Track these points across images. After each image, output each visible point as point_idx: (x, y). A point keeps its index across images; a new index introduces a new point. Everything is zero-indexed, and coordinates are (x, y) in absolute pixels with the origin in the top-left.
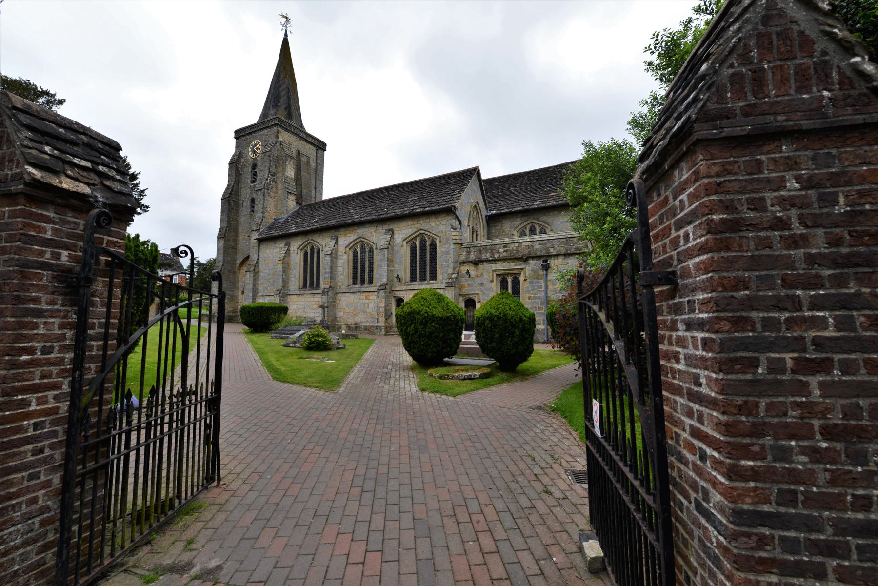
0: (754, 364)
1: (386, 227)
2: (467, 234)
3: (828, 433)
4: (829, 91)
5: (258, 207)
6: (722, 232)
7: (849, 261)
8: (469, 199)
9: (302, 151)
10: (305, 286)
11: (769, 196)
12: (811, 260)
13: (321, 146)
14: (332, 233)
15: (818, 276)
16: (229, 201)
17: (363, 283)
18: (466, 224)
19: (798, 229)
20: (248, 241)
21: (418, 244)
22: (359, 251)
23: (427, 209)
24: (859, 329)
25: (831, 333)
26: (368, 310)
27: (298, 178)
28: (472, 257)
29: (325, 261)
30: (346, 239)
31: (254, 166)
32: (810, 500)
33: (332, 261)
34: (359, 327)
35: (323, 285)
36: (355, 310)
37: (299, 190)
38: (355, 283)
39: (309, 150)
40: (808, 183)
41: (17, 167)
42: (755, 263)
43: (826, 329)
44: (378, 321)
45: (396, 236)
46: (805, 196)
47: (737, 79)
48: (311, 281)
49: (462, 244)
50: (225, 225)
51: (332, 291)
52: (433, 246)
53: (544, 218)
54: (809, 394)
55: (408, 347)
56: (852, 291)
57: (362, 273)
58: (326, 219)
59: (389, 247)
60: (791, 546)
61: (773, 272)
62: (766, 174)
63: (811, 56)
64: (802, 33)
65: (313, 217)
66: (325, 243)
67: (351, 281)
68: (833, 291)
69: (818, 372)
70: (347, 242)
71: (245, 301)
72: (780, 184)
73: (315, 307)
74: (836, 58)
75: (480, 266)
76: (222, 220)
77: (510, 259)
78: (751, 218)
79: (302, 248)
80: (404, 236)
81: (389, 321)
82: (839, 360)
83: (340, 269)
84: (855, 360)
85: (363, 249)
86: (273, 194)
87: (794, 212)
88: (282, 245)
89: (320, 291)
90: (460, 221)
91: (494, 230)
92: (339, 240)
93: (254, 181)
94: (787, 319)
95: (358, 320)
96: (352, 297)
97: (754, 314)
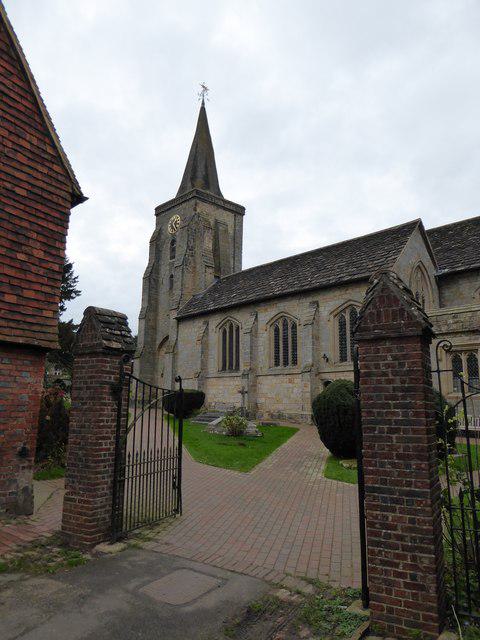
1: (310, 299)
3: (399, 457)
5: (177, 285)
7: (408, 390)
9: (220, 219)
10: (224, 368)
12: (394, 388)
13: (238, 211)
14: (250, 310)
17: (286, 363)
19: (391, 377)
20: (167, 321)
23: (356, 277)
25: (400, 418)
27: (216, 250)
29: (244, 339)
30: (267, 314)
31: (173, 242)
32: (392, 483)
33: (251, 339)
35: (242, 367)
37: (217, 261)
38: (277, 364)
39: (227, 218)
40: (395, 358)
42: (375, 390)
45: (321, 309)
47: (371, 314)
48: (230, 363)
51: (252, 373)
55: (324, 438)
57: (285, 352)
58: (246, 292)
60: (385, 500)
65: (232, 292)
66: (244, 319)
67: (273, 361)
70: (268, 318)
71: (166, 384)
72: (385, 358)
77: (463, 332)
79: (221, 326)
85: (285, 325)
88: (201, 324)
89: (240, 374)
91: (447, 293)
93: (173, 257)
95: (281, 407)
96: (274, 380)
97: (374, 410)
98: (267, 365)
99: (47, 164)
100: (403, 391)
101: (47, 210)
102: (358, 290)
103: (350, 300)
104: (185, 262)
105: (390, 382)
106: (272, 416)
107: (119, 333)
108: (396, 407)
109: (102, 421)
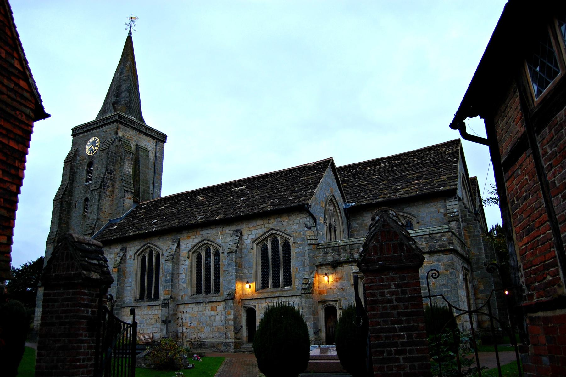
0: (382, 353)
1: (234, 228)
2: (323, 232)
8: (327, 187)
10: (142, 298)
11: (386, 291)
12: (399, 314)
13: (161, 138)
15: (401, 320)
16: (62, 202)
17: (208, 291)
18: (322, 221)
19: (395, 303)
21: (269, 246)
22: (203, 255)
25: (405, 340)
26: (215, 324)
28: (330, 258)
29: (165, 266)
30: (189, 242)
31: (90, 164)
34: (204, 344)
35: (162, 296)
36: (199, 323)
39: (148, 144)
40: (397, 286)
41: (77, 270)
43: (404, 338)
44: (226, 337)
45: (245, 237)
46: (397, 291)
49: (318, 245)
50: (56, 229)
51: (173, 303)
52: (287, 246)
53: (409, 209)
54: (399, 362)
57: (208, 281)
59: (237, 250)
62: (385, 283)
63: (397, 240)
64: (394, 231)
66: (165, 246)
67: (194, 289)
70: (190, 245)
72: (389, 287)
73: (153, 321)
75: (340, 269)
76: (52, 223)
80: (254, 237)
81: (239, 335)
83: (183, 276)
86: (108, 193)
87: (393, 297)
90: (314, 219)
91: (354, 225)
92: (181, 243)
95: (202, 336)
97: (382, 334)
98: (189, 294)
99: (13, 78)
101: (8, 126)
102: (279, 219)
103: (272, 229)
104: (103, 185)
105: (394, 308)
106: (192, 345)
107: (96, 262)
108: (401, 330)
109: (79, 360)
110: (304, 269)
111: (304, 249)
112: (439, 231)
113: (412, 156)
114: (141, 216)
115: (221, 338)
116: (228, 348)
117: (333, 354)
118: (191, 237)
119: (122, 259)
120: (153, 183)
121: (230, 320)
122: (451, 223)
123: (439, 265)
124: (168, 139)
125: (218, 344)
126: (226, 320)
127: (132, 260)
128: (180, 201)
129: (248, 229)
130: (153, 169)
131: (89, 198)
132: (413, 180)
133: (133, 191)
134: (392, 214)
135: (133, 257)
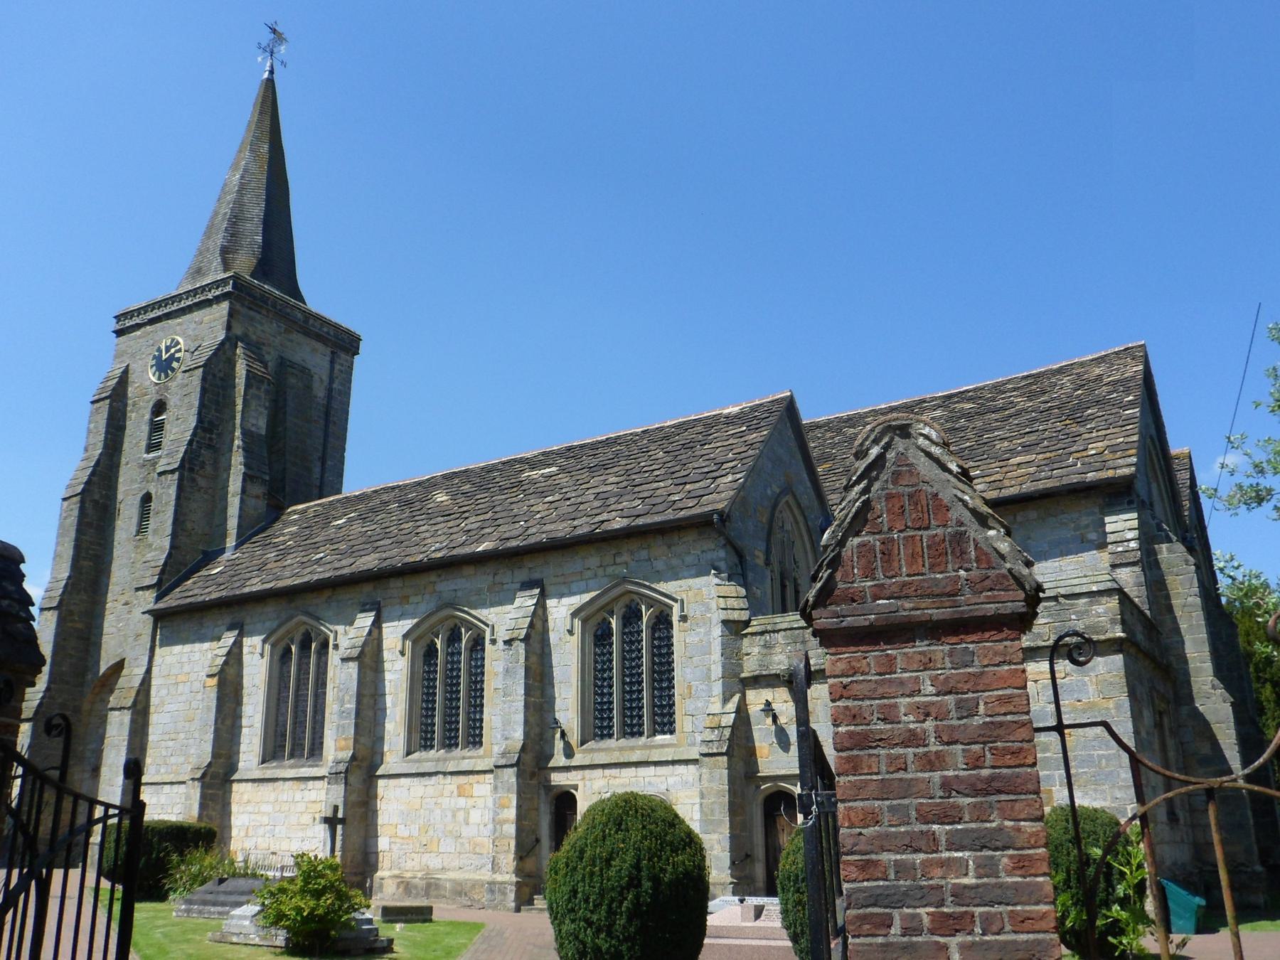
4: (967, 570)
6: (848, 749)
12: (946, 785)
13: (344, 344)
18: (760, 561)
19: (934, 747)
23: (640, 521)
24: (1002, 874)
26: (466, 831)
31: (160, 407)
34: (437, 886)
36: (425, 829)
39: (315, 358)
44: (495, 867)
46: (941, 704)
51: (363, 773)
56: (994, 825)
61: (906, 801)
68: (973, 825)
69: (957, 931)
73: (306, 819)
74: (973, 530)
78: (881, 732)
82: (981, 914)
84: (996, 914)
87: (929, 724)
93: (152, 446)
94: (923, 862)
95: (434, 862)
96: (417, 786)
97: (885, 857)
100: (976, 792)
102: (644, 554)
110: (710, 690)
111: (708, 633)
112: (1084, 589)
113: (1015, 389)
114: (285, 542)
115: (483, 870)
116: (498, 897)
117: (770, 924)
118: (412, 599)
119: (229, 653)
120: (323, 460)
121: (506, 821)
122: (1118, 571)
123: (1085, 684)
124: (363, 346)
125: (474, 886)
126: (498, 823)
127: (257, 656)
128: (386, 503)
129: (561, 579)
130: (322, 422)
131: (153, 493)
132: (1013, 452)
133: (267, 478)
134: (927, 437)
135: (259, 650)
